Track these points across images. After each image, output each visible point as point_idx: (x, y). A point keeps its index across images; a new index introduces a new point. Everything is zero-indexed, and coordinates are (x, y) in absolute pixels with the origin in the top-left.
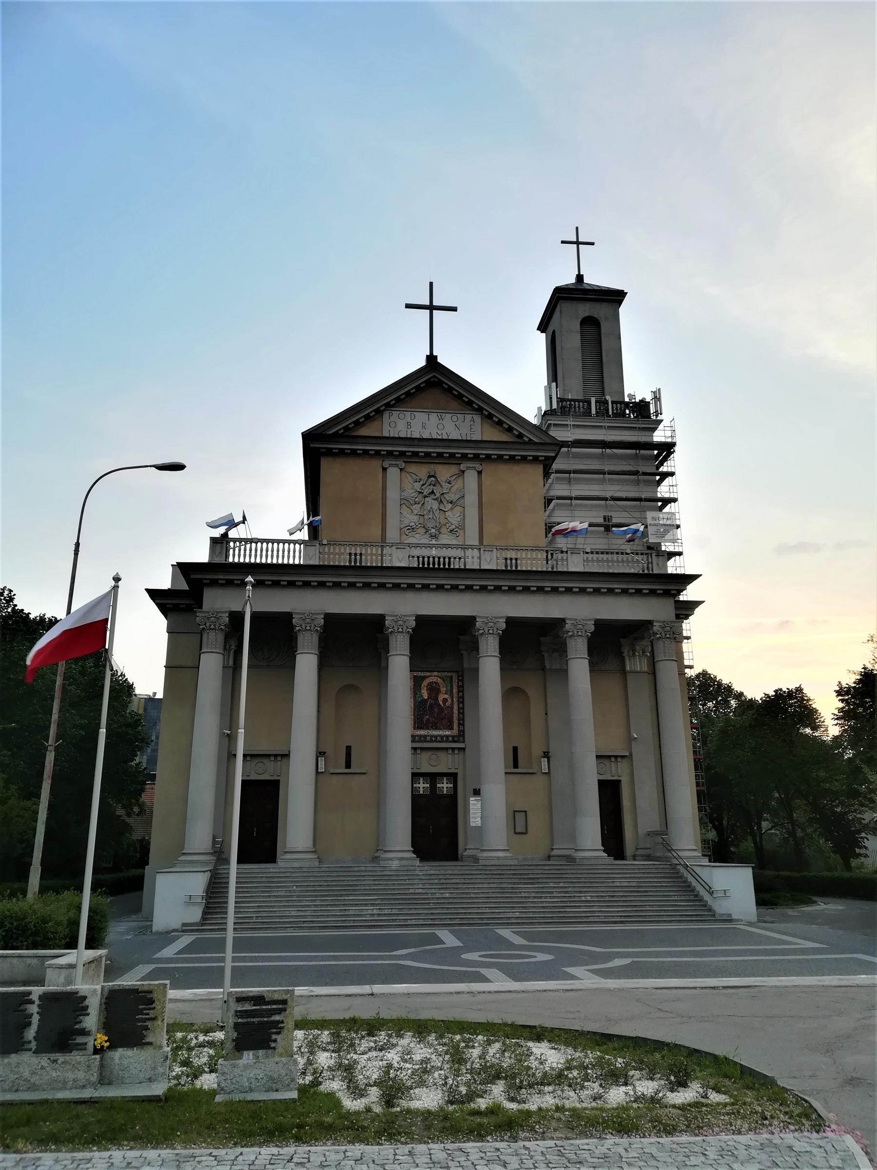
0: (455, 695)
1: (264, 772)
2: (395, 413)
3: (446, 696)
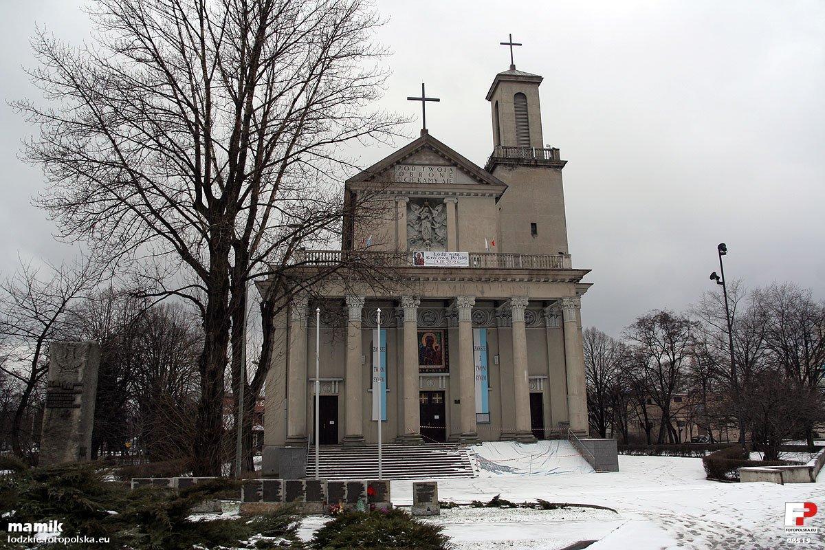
0: (443, 344)
1: (332, 391)
3: (437, 345)
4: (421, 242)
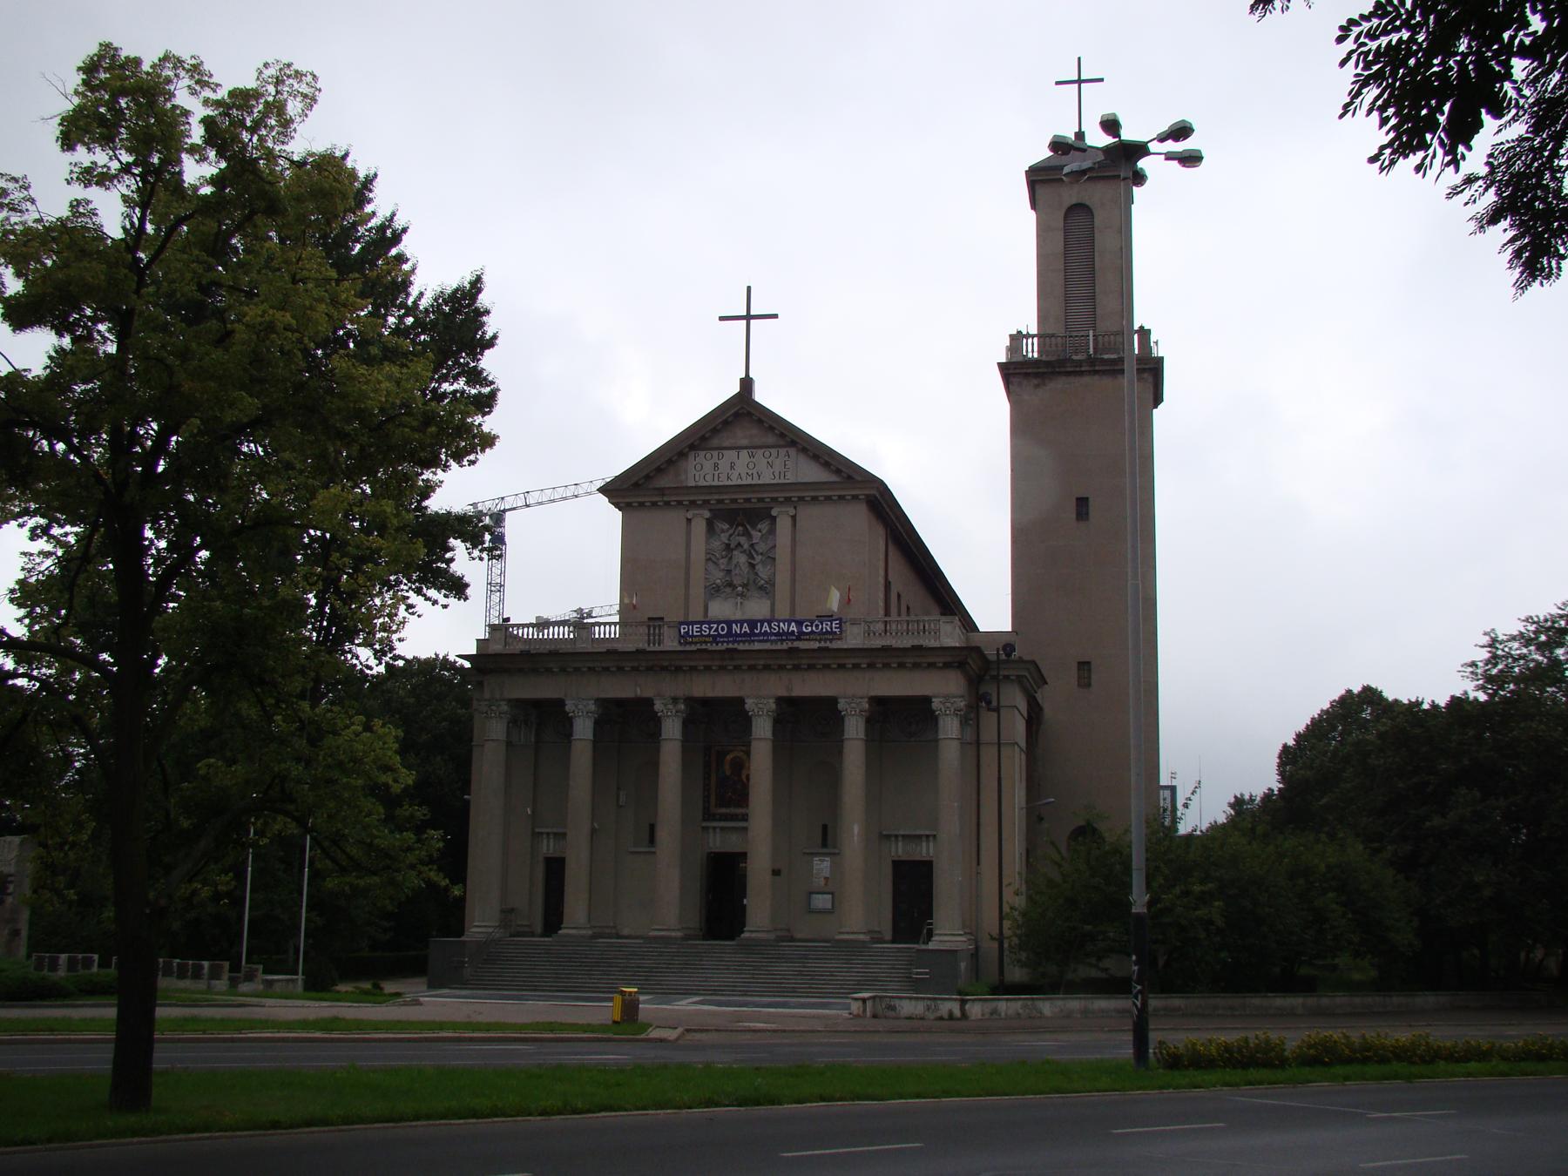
2: (702, 453)
4: (728, 590)
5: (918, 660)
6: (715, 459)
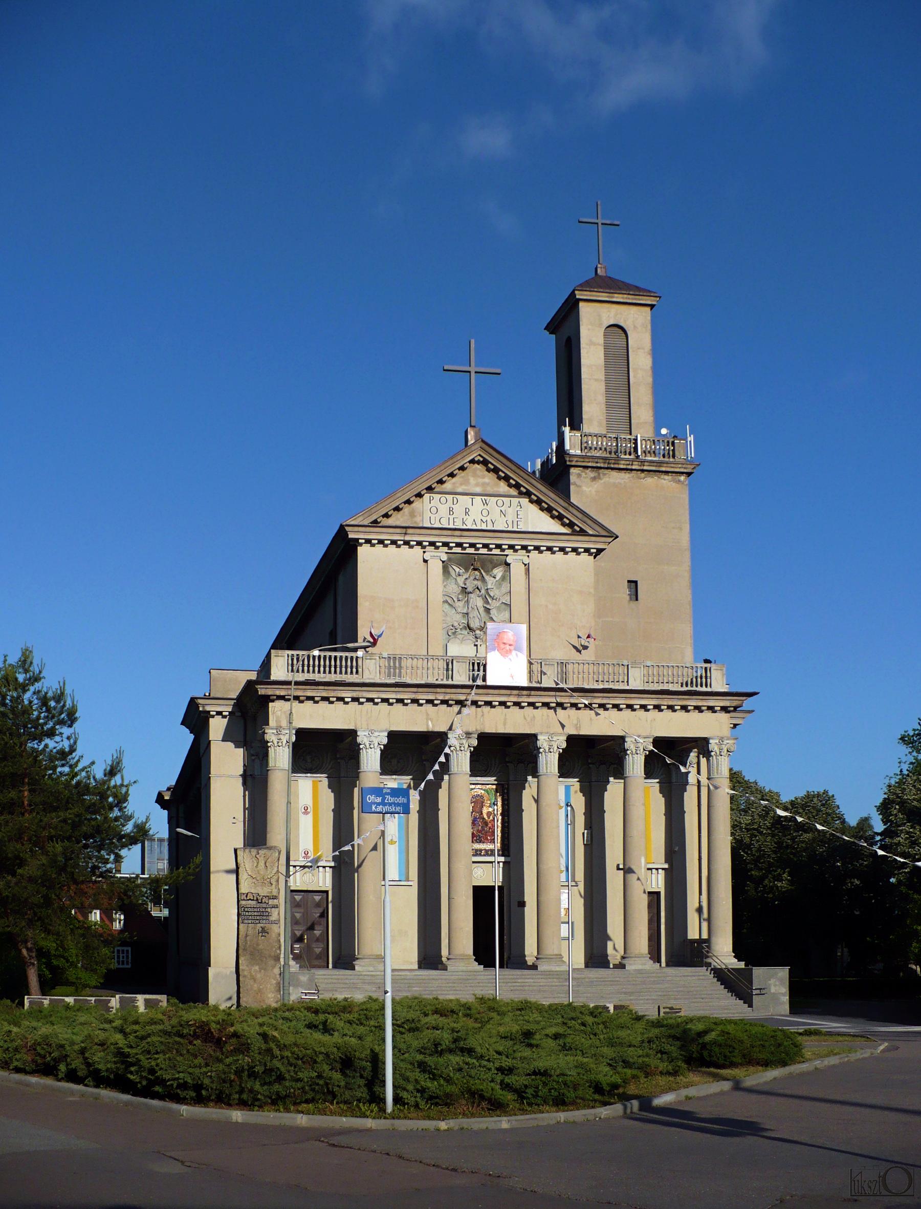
5: (700, 703)
6: (450, 503)
